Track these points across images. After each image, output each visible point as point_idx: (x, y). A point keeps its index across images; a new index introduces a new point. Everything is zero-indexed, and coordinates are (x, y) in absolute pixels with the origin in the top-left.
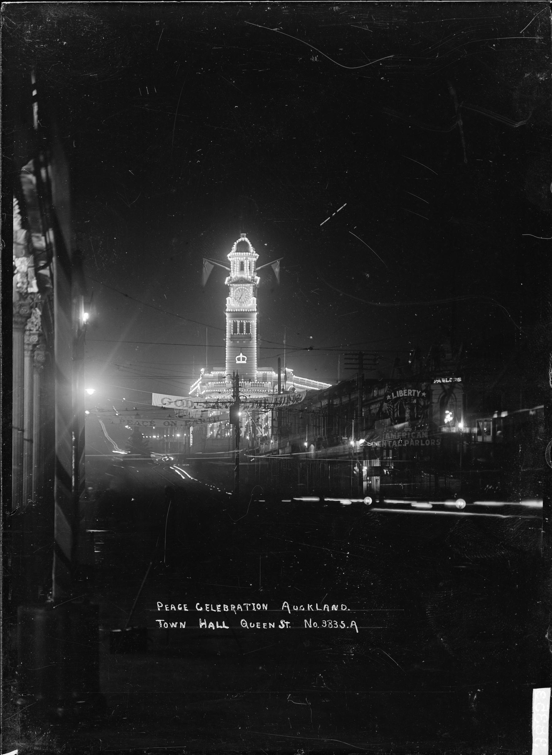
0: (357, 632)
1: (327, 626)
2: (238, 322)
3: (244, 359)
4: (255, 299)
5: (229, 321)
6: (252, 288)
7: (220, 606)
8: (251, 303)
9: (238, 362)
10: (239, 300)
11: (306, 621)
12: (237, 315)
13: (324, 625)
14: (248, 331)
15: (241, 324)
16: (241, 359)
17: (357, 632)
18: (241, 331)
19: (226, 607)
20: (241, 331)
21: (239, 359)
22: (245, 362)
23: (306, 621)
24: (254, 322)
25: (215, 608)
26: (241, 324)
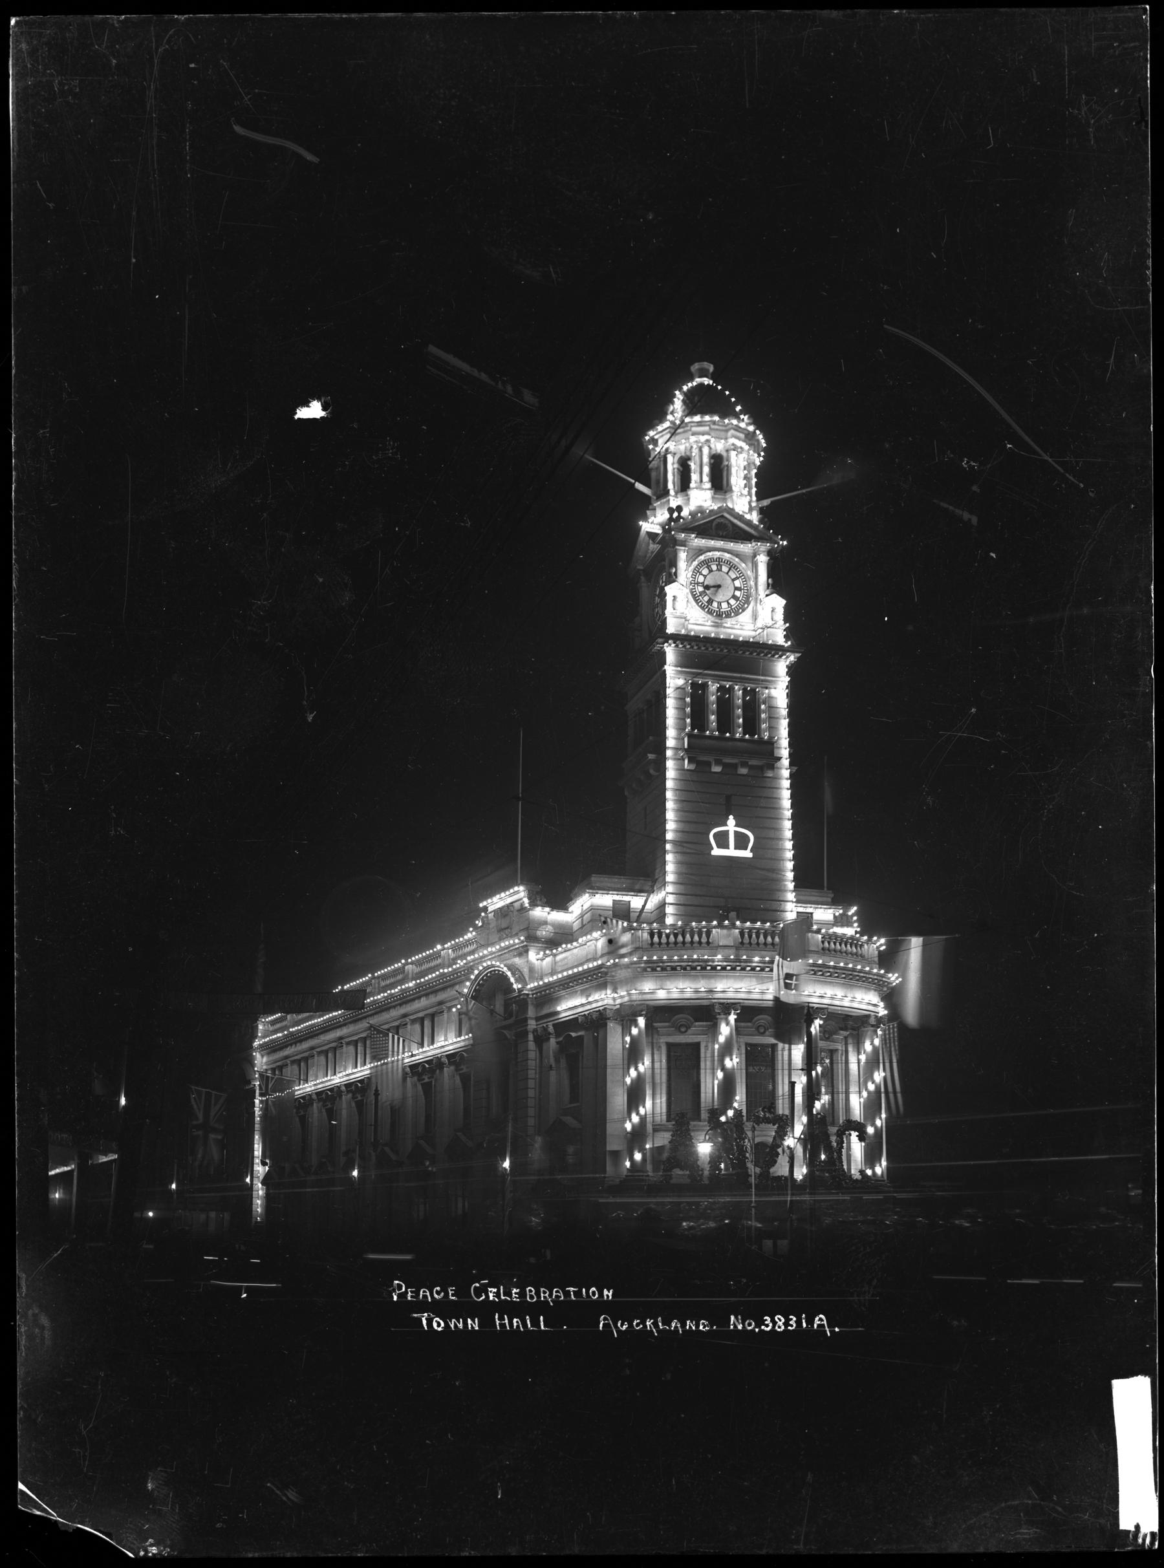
0: (1132, 1401)
1: (774, 1326)
2: (713, 687)
3: (741, 842)
4: (778, 603)
5: (674, 679)
6: (762, 559)
7: (711, 369)
8: (765, 617)
9: (717, 852)
10: (705, 594)
11: (732, 1318)
12: (708, 654)
13: (767, 1326)
14: (752, 724)
15: (725, 705)
16: (730, 841)
17: (1132, 1401)
18: (725, 722)
19: (780, 1320)
20: (725, 722)
21: (722, 840)
22: (747, 854)
23: (732, 1318)
24: (779, 693)
25: (508, 1293)
26: (725, 705)
